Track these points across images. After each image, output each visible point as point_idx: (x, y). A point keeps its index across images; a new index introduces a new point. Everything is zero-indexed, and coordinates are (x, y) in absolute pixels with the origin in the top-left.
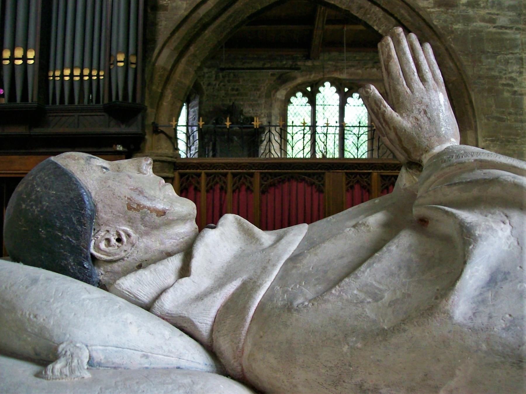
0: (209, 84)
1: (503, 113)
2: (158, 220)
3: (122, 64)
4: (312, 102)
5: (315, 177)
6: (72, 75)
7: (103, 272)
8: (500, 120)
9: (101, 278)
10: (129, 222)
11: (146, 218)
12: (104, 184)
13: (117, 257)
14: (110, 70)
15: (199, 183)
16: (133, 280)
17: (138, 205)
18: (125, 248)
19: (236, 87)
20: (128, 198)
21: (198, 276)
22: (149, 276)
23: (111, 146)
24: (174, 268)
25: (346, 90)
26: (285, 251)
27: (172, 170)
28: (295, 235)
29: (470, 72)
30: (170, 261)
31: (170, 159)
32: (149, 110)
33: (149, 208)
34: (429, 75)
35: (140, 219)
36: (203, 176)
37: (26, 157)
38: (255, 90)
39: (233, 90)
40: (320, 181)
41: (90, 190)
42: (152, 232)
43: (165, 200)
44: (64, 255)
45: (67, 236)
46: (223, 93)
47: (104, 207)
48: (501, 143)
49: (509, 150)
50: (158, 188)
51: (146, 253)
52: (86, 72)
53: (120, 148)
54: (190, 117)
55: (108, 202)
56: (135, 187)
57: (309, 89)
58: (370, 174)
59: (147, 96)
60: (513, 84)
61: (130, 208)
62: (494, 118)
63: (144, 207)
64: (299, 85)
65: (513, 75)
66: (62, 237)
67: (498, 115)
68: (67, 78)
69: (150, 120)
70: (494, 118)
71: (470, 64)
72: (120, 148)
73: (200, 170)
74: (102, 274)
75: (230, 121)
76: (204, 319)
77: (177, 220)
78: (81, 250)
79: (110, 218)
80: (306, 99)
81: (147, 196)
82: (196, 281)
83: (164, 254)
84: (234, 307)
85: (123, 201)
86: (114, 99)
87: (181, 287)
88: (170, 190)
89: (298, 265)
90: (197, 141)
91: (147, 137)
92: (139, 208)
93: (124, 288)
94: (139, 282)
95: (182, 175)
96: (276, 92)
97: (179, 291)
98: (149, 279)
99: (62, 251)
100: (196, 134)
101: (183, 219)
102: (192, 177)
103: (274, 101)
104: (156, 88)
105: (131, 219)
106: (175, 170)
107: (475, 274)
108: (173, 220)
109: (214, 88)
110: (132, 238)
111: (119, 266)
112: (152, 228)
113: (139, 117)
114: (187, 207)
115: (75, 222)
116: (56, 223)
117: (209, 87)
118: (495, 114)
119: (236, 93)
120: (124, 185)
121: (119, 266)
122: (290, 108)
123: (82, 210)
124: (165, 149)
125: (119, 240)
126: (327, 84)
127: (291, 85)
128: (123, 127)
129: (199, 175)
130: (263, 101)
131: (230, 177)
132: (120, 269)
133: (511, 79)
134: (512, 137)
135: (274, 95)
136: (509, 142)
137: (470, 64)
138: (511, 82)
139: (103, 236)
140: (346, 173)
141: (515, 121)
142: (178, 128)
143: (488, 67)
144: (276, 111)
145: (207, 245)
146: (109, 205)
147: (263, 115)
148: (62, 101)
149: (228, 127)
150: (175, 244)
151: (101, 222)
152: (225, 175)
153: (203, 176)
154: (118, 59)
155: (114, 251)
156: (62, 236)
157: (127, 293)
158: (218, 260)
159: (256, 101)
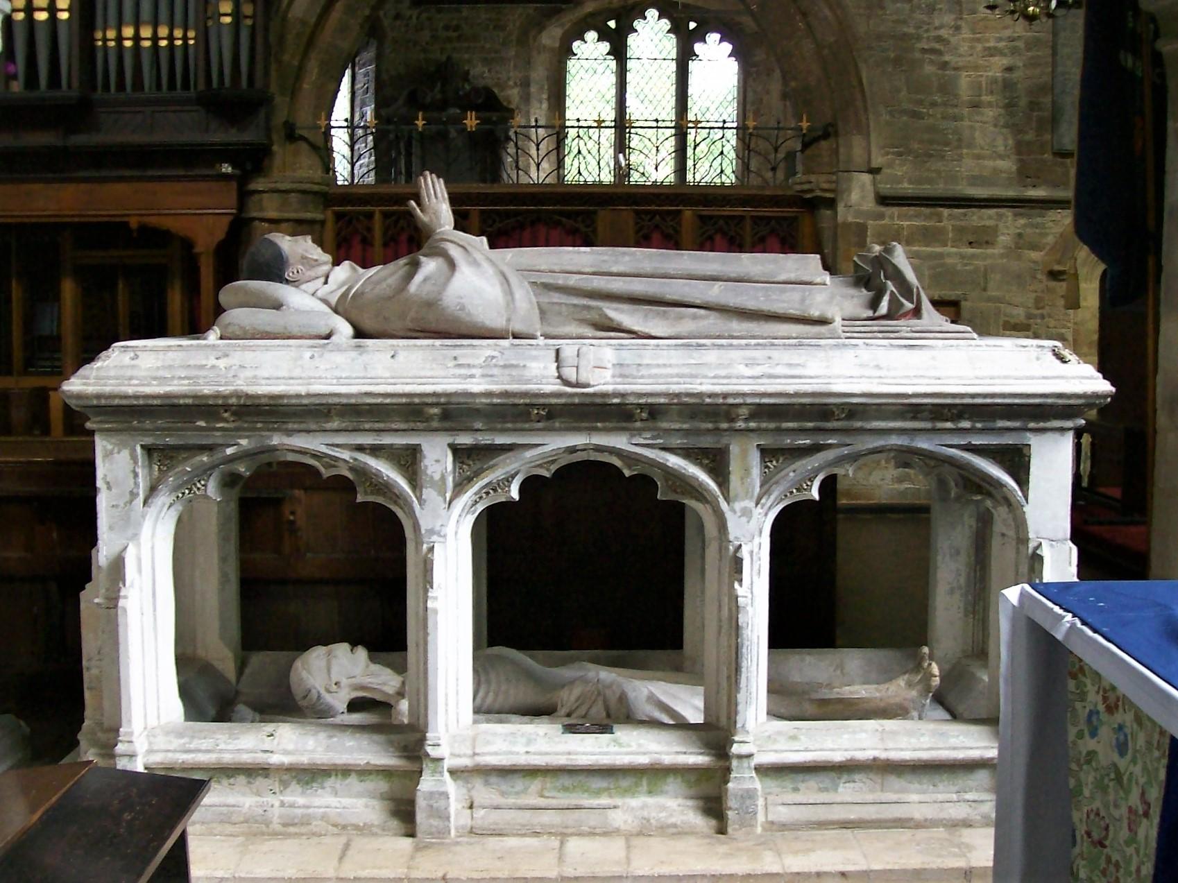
0: (397, 16)
1: (920, 102)
3: (228, 20)
4: (619, 53)
5: (580, 219)
6: (137, 38)
8: (916, 115)
14: (206, 29)
15: (369, 229)
19: (455, 22)
23: (212, 166)
25: (692, 25)
29: (862, 28)
31: (316, 188)
32: (278, 100)
34: (439, 195)
36: (377, 217)
37: (56, 186)
38: (495, 27)
39: (447, 28)
40: (588, 226)
46: (426, 35)
48: (916, 157)
49: (928, 170)
52: (163, 31)
53: (227, 169)
54: (358, 86)
57: (612, 24)
58: (680, 211)
59: (273, 74)
60: (942, 48)
62: (904, 112)
64: (592, 15)
65: (943, 33)
67: (911, 107)
68: (128, 44)
69: (280, 117)
70: (904, 112)
71: (862, 11)
72: (227, 169)
76: (334, 300)
80: (605, 47)
84: (344, 295)
86: (215, 84)
88: (319, 250)
91: (275, 148)
95: (339, 216)
96: (540, 32)
101: (325, 263)
102: (358, 219)
103: (534, 53)
104: (290, 57)
107: (418, 278)
109: (407, 25)
113: (262, 115)
114: (328, 258)
117: (398, 23)
118: (905, 106)
119: (455, 34)
122: (572, 65)
126: (652, 13)
127: (571, 17)
128: (234, 131)
129: (370, 216)
130: (512, 53)
133: (939, 39)
134: (935, 146)
135: (535, 39)
136: (931, 156)
137: (862, 11)
138: (937, 46)
140: (637, 213)
141: (943, 118)
142: (333, 132)
143: (895, 17)
144: (539, 73)
147: (511, 83)
148: (121, 86)
153: (377, 217)
154: (222, 10)
159: (496, 52)
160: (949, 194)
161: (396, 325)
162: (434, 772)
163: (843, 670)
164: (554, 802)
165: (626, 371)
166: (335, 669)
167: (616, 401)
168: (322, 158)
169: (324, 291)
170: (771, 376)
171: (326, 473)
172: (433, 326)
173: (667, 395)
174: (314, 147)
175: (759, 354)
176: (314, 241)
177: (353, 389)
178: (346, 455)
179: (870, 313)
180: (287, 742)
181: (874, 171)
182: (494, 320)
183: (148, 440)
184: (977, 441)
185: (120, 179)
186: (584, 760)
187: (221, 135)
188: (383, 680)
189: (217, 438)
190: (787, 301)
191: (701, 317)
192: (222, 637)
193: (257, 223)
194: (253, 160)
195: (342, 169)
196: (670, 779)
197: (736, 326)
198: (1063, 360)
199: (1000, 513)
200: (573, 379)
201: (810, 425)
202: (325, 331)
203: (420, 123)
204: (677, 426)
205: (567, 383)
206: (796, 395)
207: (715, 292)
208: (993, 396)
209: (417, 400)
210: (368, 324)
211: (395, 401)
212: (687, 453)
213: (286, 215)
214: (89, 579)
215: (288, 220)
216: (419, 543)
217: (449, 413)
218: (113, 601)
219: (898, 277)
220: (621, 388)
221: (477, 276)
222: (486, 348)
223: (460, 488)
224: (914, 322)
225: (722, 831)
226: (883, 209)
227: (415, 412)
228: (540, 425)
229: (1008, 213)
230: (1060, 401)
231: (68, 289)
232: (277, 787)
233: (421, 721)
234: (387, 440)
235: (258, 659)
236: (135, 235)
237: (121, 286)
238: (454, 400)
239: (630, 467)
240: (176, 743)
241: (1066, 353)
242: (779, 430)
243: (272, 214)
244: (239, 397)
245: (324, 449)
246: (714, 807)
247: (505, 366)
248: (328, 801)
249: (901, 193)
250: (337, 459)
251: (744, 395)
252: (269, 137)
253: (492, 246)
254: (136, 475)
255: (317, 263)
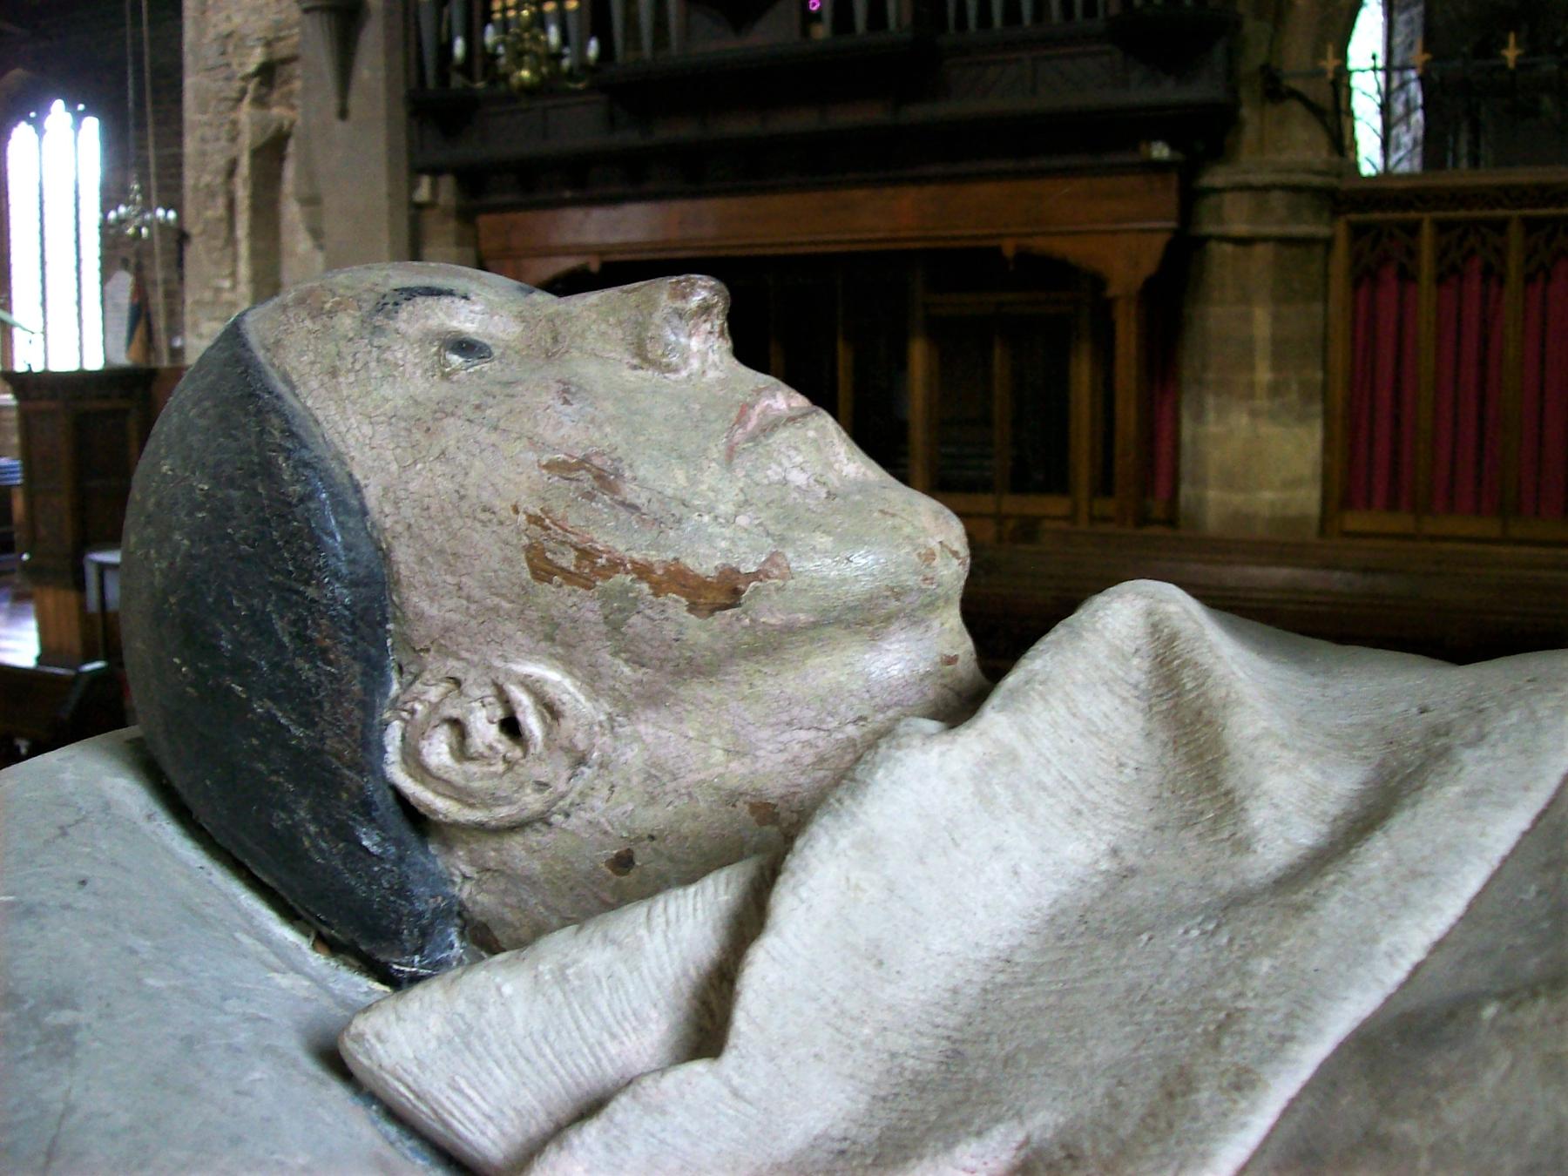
2: (700, 632)
7: (468, 870)
9: (464, 895)
10: (550, 638)
11: (635, 619)
12: (424, 442)
13: (503, 812)
15: (1412, 253)
16: (435, 1024)
17: (586, 554)
18: (543, 772)
20: (534, 520)
21: (772, 1059)
22: (519, 1011)
24: (671, 971)
26: (1359, 948)
27: (1326, 215)
28: (1475, 796)
30: (659, 920)
31: (1317, 181)
32: (1250, 26)
33: (643, 571)
35: (603, 628)
36: (1427, 231)
37: (889, 192)
41: (358, 476)
42: (683, 692)
43: (742, 520)
44: (274, 787)
45: (269, 704)
47: (422, 560)
50: (717, 450)
51: (652, 800)
53: (1160, 151)
54: (1398, 40)
55: (439, 537)
56: (579, 454)
61: (543, 570)
63: (615, 565)
66: (245, 706)
69: (1254, 58)
72: (1160, 151)
73: (1417, 209)
74: (465, 877)
75: (1518, 44)
77: (815, 625)
78: (335, 772)
79: (456, 617)
81: (641, 501)
82: (752, 1091)
83: (743, 809)
85: (505, 532)
87: (648, 1122)
89: (1408, 1128)
90: (1418, 116)
91: (1246, 112)
92: (591, 568)
93: (386, 1062)
94: (464, 1038)
95: (1357, 231)
97: (637, 1147)
98: (519, 1028)
99: (261, 766)
100: (1415, 91)
101: (866, 617)
105: (558, 625)
106: (1335, 213)
108: (790, 630)
110: (567, 724)
111: (530, 851)
112: (678, 673)
113: (1218, 52)
114: (928, 539)
115: (286, 639)
116: (218, 635)
120: (519, 446)
121: (530, 851)
123: (307, 583)
124: (1301, 146)
125: (511, 726)
129: (1413, 229)
131: (1515, 236)
132: (537, 866)
139: (434, 707)
145: (870, 847)
146: (441, 552)
149: (1511, 65)
150: (809, 757)
151: (419, 633)
152: (1501, 226)
153: (1427, 231)
155: (487, 784)
156: (249, 700)
157: (408, 1094)
158: (938, 944)
168: (1328, 130)
174: (1315, 110)
176: (752, 344)
185: (983, 177)
187: (1147, 91)
194: (1207, 135)
195: (1369, 156)
203: (1511, 54)
215: (1265, 239)
231: (919, 354)
237: (998, 352)
243: (1240, 228)
252: (1234, 91)
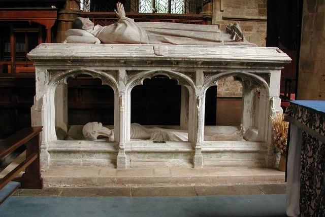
84: (98, 33)
107: (118, 28)
160: (240, 17)
161: (111, 41)
162: (121, 152)
163: (223, 130)
164: (151, 160)
165: (171, 52)
166: (94, 128)
167: (169, 59)
169: (92, 32)
170: (207, 54)
171: (94, 77)
172: (121, 41)
173: (181, 58)
175: (205, 49)
177: (103, 56)
178: (100, 73)
179: (231, 40)
180: (84, 145)
181: (222, 11)
182: (138, 40)
183: (49, 68)
184: (258, 72)
186: (158, 150)
188: (106, 131)
189: (67, 68)
190: (210, 36)
191: (189, 40)
192: (64, 121)
193: (62, 22)
196: (180, 154)
197: (198, 42)
198: (279, 52)
199: (262, 91)
200: (158, 54)
201: (217, 67)
202: (94, 42)
204: (184, 66)
205: (156, 55)
206: (214, 59)
207: (192, 34)
208: (262, 60)
209: (118, 58)
210: (104, 40)
211: (113, 58)
212: (186, 73)
213: (70, 20)
214: (33, 104)
216: (118, 95)
217: (126, 62)
218: (40, 111)
219: (238, 31)
220: (170, 56)
221: (132, 29)
222: (135, 46)
223: (128, 81)
224: (241, 42)
225: (193, 167)
226: (224, 21)
227: (117, 61)
228: (149, 65)
229: (256, 23)
230: (279, 62)
232: (81, 156)
233: (118, 140)
234: (110, 69)
235: (72, 127)
236: (30, 24)
238: (128, 58)
239: (171, 77)
240: (56, 145)
241: (280, 50)
242: (209, 68)
243: (66, 19)
244: (73, 57)
245: (93, 71)
246: (191, 161)
247: (140, 50)
248: (95, 159)
249: (229, 17)
250: (97, 74)
251: (200, 58)
253: (135, 21)
254: (46, 78)
255: (91, 25)
